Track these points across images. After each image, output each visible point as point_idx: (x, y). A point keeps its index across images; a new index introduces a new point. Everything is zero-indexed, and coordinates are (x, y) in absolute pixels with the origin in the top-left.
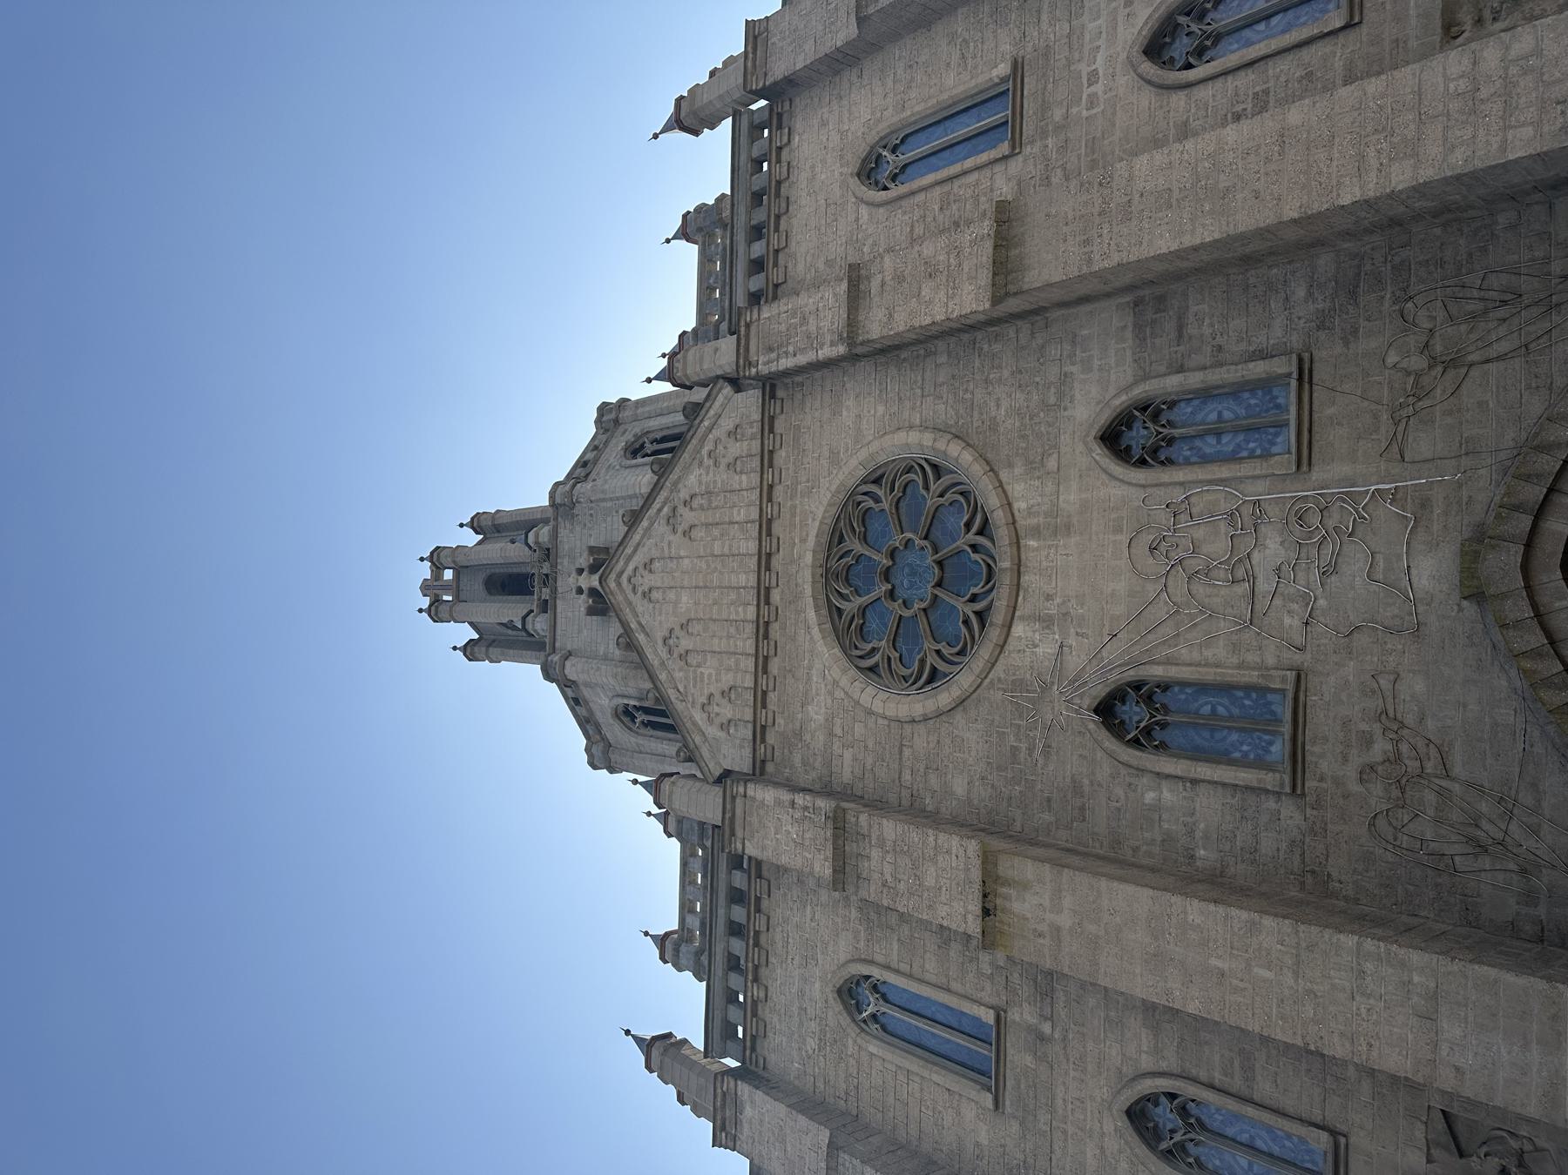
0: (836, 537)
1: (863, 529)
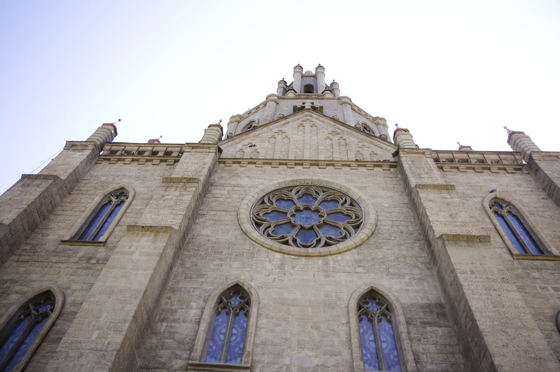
0: (325, 189)
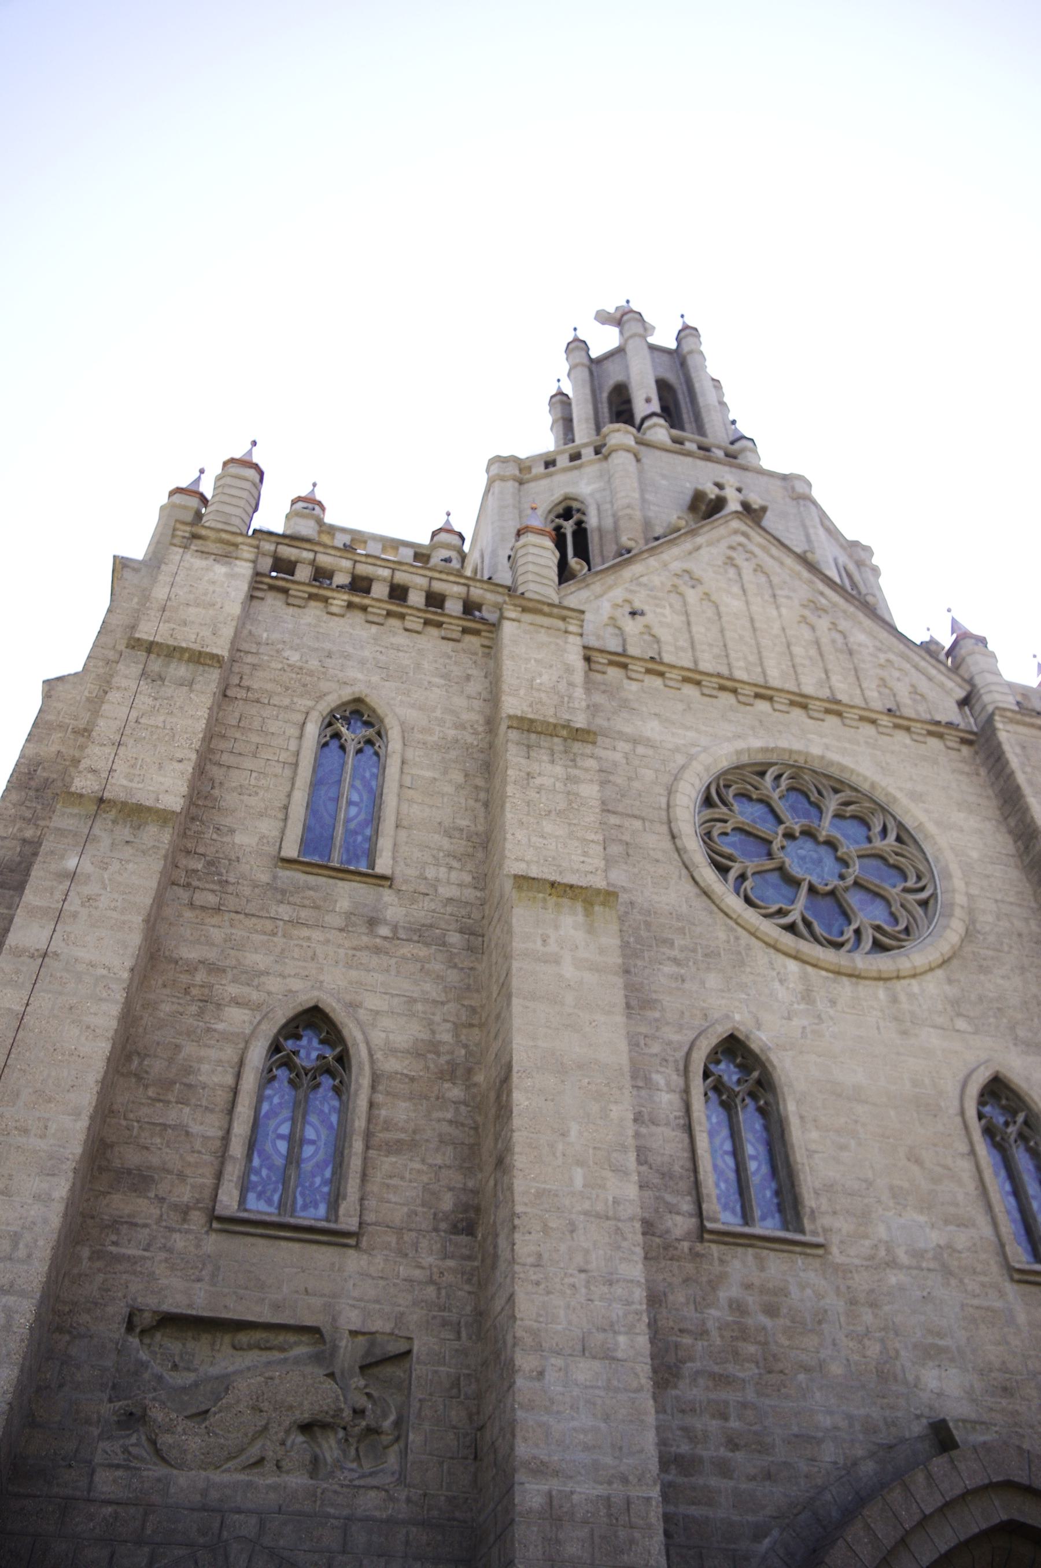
1: (848, 815)
